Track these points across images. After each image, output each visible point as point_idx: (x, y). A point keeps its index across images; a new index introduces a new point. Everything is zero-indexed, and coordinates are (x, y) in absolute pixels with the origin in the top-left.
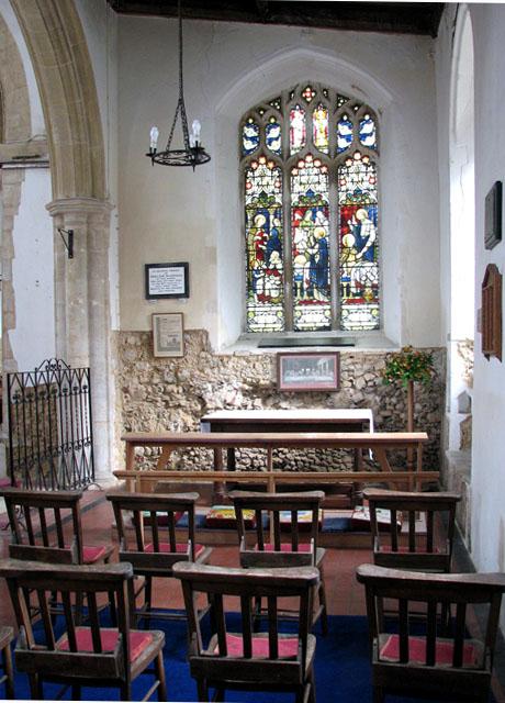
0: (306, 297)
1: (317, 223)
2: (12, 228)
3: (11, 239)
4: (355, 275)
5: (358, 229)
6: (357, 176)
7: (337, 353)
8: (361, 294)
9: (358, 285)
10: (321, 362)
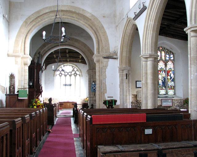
0: (161, 88)
1: (163, 74)
2: (106, 71)
3: (105, 73)
4: (170, 84)
5: (170, 75)
6: (170, 65)
7: (172, 99)
8: (171, 88)
9: (171, 86)
10: (169, 101)
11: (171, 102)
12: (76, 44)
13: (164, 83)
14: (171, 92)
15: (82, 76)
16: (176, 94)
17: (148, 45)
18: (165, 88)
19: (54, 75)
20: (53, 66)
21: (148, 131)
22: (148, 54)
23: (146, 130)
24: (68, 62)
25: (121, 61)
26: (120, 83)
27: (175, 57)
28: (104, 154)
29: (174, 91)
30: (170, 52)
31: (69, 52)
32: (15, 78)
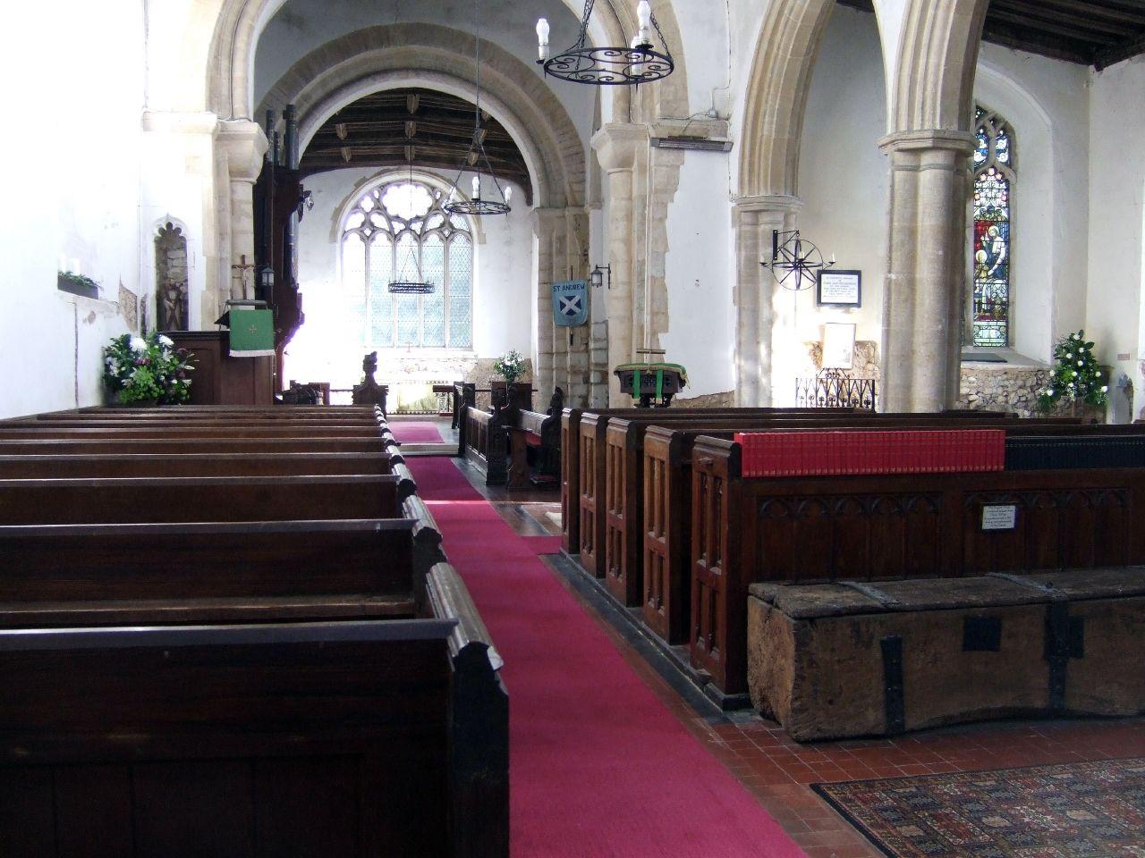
9: (989, 302)
12: (477, 66)
15: (483, 241)
17: (930, 87)
19: (333, 233)
20: (475, 181)
21: (999, 517)
22: (929, 134)
23: (986, 509)
24: (406, 163)
25: (751, 164)
26: (739, 282)
28: (807, 623)
29: (1003, 329)
30: (995, 120)
31: (422, 111)
32: (190, 246)
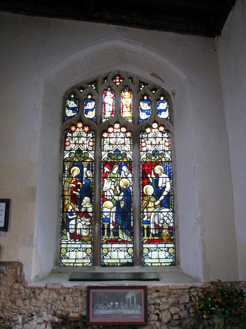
0: (112, 237)
4: (153, 219)
5: (156, 182)
6: (155, 141)
7: (145, 288)
11: (139, 302)
13: (127, 214)
14: (157, 255)
16: (182, 263)
18: (132, 234)
27: (175, 108)
29: (171, 251)
